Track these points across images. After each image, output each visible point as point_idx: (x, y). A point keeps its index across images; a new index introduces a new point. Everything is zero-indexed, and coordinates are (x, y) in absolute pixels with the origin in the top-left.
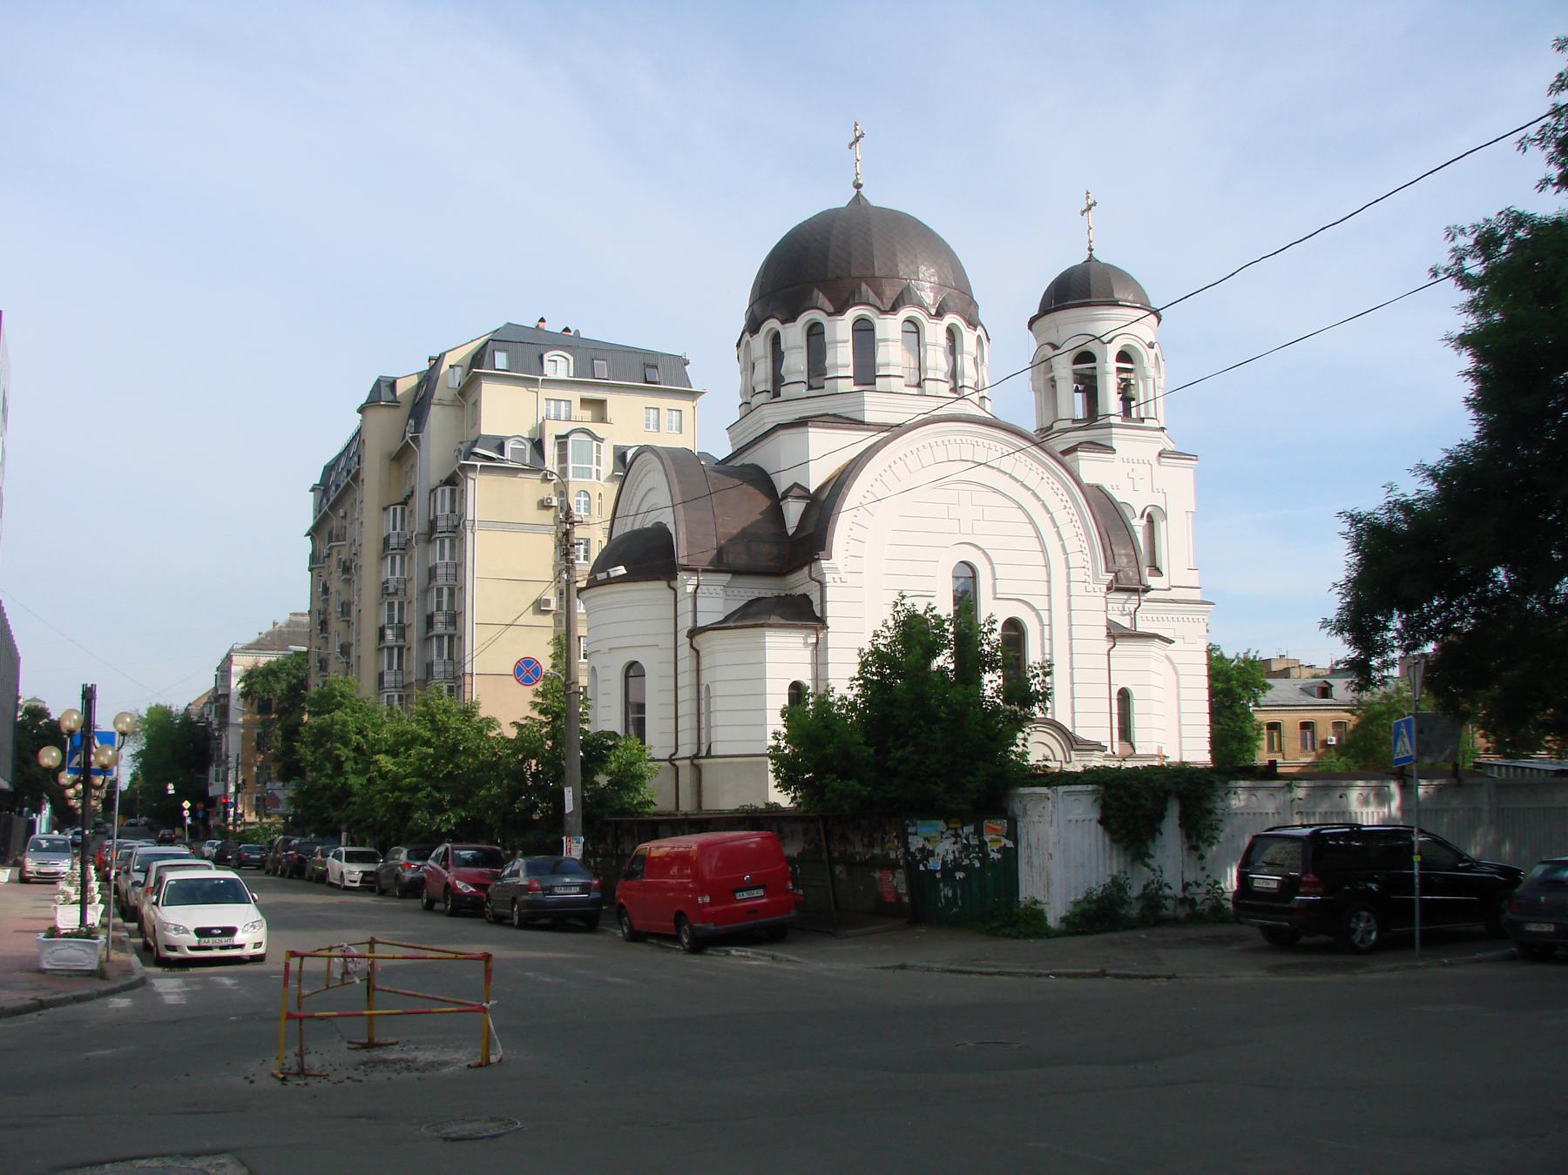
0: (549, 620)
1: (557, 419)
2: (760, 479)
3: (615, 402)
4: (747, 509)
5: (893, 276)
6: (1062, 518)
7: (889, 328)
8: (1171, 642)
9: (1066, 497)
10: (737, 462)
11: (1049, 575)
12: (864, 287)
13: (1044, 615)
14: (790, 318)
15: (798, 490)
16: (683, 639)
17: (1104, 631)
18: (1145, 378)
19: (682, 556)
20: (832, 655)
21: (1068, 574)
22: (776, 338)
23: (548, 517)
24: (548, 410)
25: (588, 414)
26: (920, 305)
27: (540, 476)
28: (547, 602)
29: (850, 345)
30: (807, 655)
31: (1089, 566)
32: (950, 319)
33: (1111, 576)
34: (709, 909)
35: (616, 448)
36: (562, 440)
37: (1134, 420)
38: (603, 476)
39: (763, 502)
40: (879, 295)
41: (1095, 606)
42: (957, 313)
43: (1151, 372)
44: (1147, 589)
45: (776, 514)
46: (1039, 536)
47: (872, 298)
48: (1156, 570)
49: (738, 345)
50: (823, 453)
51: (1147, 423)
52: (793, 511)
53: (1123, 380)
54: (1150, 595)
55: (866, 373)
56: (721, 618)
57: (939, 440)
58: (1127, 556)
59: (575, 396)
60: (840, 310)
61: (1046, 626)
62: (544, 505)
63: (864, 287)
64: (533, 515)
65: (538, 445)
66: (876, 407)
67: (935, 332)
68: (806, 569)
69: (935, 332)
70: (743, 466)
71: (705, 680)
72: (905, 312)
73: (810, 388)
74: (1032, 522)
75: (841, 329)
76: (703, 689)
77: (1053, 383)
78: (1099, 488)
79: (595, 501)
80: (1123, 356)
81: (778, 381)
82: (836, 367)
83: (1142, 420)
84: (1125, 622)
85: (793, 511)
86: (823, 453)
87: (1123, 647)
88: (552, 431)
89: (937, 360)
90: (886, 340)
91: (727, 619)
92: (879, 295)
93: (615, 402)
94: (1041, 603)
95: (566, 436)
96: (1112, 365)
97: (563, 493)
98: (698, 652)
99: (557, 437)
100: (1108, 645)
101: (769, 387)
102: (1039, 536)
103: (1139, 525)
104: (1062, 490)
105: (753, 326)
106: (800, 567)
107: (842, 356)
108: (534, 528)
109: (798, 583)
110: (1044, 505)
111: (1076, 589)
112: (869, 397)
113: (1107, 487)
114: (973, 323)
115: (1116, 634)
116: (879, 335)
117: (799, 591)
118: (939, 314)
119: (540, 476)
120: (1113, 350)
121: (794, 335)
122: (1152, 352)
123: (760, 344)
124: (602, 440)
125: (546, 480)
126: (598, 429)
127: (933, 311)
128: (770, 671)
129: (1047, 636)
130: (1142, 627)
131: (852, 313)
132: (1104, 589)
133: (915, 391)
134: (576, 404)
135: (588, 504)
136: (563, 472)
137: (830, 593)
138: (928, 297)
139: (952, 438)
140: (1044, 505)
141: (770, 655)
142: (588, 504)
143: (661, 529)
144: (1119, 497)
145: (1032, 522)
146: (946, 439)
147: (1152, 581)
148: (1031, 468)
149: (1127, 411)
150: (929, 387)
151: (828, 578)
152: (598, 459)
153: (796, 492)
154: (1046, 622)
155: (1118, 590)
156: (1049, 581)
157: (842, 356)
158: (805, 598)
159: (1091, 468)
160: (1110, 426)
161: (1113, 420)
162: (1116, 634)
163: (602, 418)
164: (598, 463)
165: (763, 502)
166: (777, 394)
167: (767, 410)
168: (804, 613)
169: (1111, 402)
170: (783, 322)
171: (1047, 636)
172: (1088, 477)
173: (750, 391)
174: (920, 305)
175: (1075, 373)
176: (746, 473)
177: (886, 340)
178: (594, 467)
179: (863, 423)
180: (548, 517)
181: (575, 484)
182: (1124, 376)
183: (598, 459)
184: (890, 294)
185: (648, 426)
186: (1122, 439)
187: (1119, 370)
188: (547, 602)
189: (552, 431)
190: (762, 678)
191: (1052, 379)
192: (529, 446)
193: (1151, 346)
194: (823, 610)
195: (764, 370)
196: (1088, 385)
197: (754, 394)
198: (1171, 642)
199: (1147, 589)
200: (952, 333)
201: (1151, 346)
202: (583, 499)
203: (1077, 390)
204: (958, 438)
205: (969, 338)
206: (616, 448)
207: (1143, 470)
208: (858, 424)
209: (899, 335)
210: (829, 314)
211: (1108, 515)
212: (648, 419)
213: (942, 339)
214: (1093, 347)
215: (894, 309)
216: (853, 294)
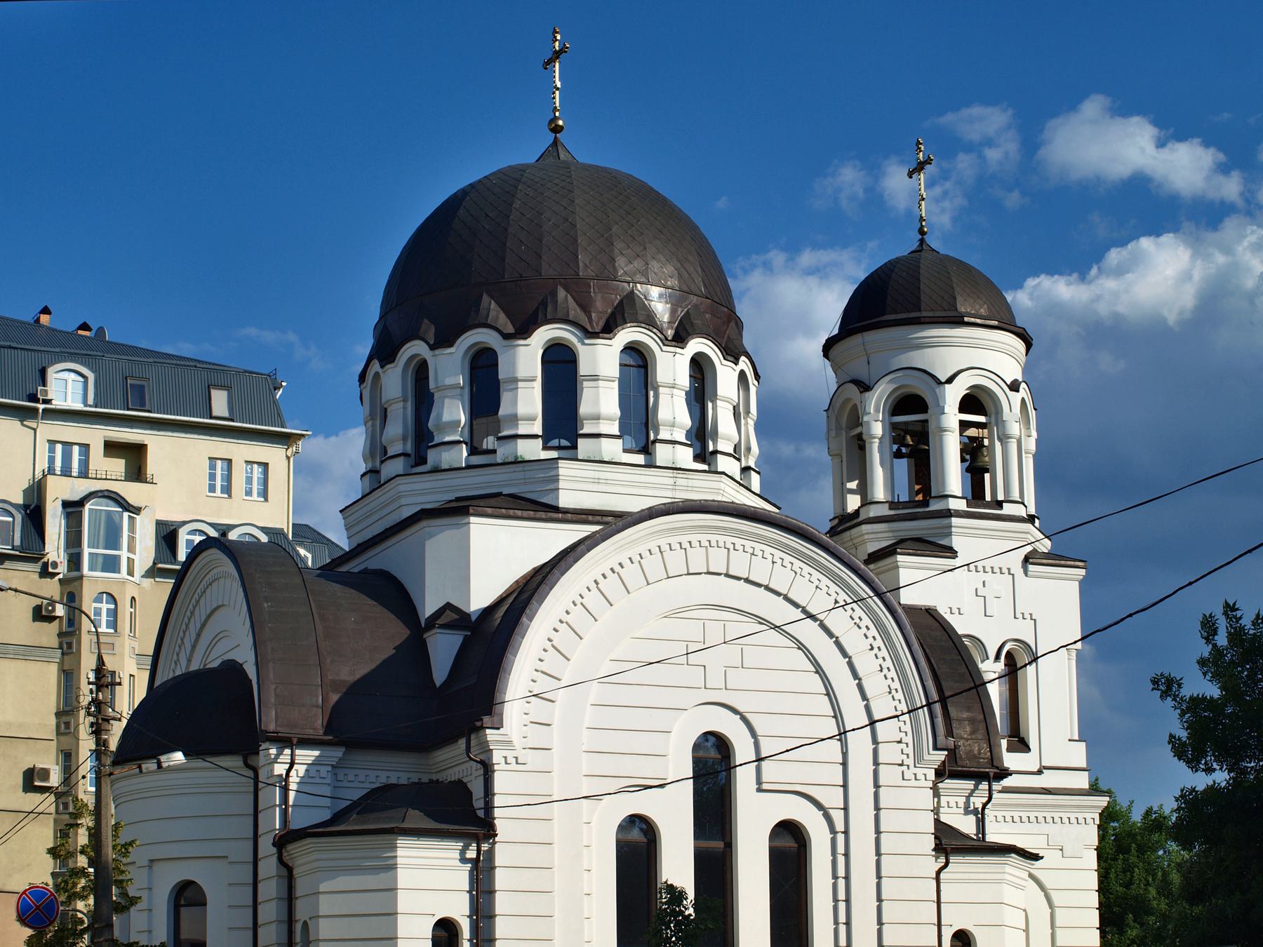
0: (47, 803)
1: (66, 472)
2: (394, 594)
3: (160, 446)
4: (367, 642)
5: (608, 275)
6: (866, 664)
7: (602, 359)
8: (1036, 857)
9: (873, 631)
10: (354, 566)
11: (845, 754)
12: (562, 293)
13: (838, 817)
14: (444, 340)
15: (453, 617)
16: (266, 847)
17: (930, 842)
18: (1004, 438)
19: (269, 721)
20: (502, 879)
21: (875, 752)
22: (421, 371)
23: (48, 634)
24: (52, 460)
25: (118, 466)
26: (649, 321)
27: (37, 567)
28: (45, 774)
29: (538, 386)
30: (461, 877)
31: (909, 739)
32: (698, 345)
33: (941, 756)
34: (1185, 166)
35: (159, 524)
36: (73, 508)
37: (988, 505)
38: (140, 569)
39: (398, 632)
40: (585, 307)
41: (917, 803)
42: (707, 336)
43: (1014, 428)
44: (1004, 773)
45: (415, 651)
46: (830, 693)
47: (575, 312)
48: (1020, 744)
49: (362, 377)
50: (496, 555)
51: (1008, 509)
52: (443, 649)
53: (971, 439)
54: (1007, 782)
55: (563, 423)
56: (326, 815)
57: (674, 541)
58: (972, 721)
59: (96, 436)
60: (524, 331)
61: (841, 834)
62: (41, 615)
63: (562, 293)
64: (21, 628)
65: (34, 513)
66: (576, 486)
67: (672, 367)
68: (462, 743)
69: (672, 367)
70: (365, 572)
71: (301, 913)
72: (627, 335)
73: (473, 451)
74: (819, 670)
75: (526, 359)
76: (298, 927)
77: (860, 444)
78: (931, 613)
79: (125, 610)
80: (973, 402)
81: (423, 438)
82: (514, 419)
83: (999, 504)
84: (967, 826)
85: (443, 649)
86: (496, 555)
87: (959, 865)
88: (59, 490)
89: (673, 411)
90: (595, 378)
91: (337, 818)
92: (585, 307)
93: (160, 446)
94: (833, 799)
95: (81, 503)
96: (952, 417)
97: (72, 600)
98: (290, 870)
99: (66, 504)
100: (933, 865)
101: (409, 448)
102: (830, 693)
103: (991, 669)
104: (866, 621)
105: (384, 351)
106: (451, 740)
107: (527, 403)
108: (27, 652)
109: (450, 762)
110: (838, 644)
111: (888, 775)
112: (566, 469)
113: (943, 611)
114: (733, 352)
115: (949, 843)
116: (583, 369)
117: (452, 775)
118: (680, 339)
119: (37, 567)
120: (953, 395)
121: (449, 368)
122: (1016, 398)
123: (394, 380)
124: (137, 510)
125: (45, 573)
126: (132, 492)
127: (670, 333)
128: (404, 902)
129: (841, 849)
130: (994, 835)
131: (544, 335)
132: (931, 775)
133: (640, 459)
134: (97, 450)
135: (114, 614)
136: (75, 561)
137: (501, 782)
138: (661, 309)
139: (694, 538)
140: (838, 644)
141: (404, 877)
142: (114, 614)
143: (232, 669)
144: (961, 626)
145: (819, 670)
146: (684, 539)
147: (1011, 760)
148: (813, 583)
149: (976, 493)
150: (663, 454)
151: (497, 757)
152: (132, 540)
153: (449, 616)
154: (840, 826)
155: (955, 775)
156: (844, 764)
157: (527, 403)
158: (461, 787)
159: (919, 582)
160: (949, 514)
161: (954, 504)
162: (949, 843)
163: (137, 472)
164: (131, 549)
165: (398, 632)
166: (422, 460)
167: (405, 485)
168: (463, 814)
169: (953, 477)
170: (433, 347)
171: (841, 849)
172: (908, 597)
173: (377, 452)
174: (649, 321)
175: (894, 426)
176: (371, 574)
177: (595, 378)
178: (124, 554)
179: (556, 509)
180: (48, 634)
181: (94, 579)
182: (972, 432)
183: (132, 540)
184: (602, 308)
185: (212, 488)
186: (969, 538)
187: (964, 425)
188: (45, 774)
189: (59, 490)
190: (391, 914)
191: (859, 437)
192: (19, 518)
193: (1014, 387)
194: (489, 807)
195: (396, 431)
196: (915, 446)
197: (386, 457)
198: (1036, 857)
199: (1004, 773)
200: (700, 366)
201: (1014, 387)
202: (105, 607)
203: (898, 455)
204: (704, 538)
205: (726, 376)
206: (159, 524)
207: (999, 584)
208: (548, 511)
209: (615, 371)
210: (507, 337)
211: (941, 655)
212: (212, 477)
213: (682, 376)
214: (919, 387)
215: (609, 329)
216: (544, 304)
